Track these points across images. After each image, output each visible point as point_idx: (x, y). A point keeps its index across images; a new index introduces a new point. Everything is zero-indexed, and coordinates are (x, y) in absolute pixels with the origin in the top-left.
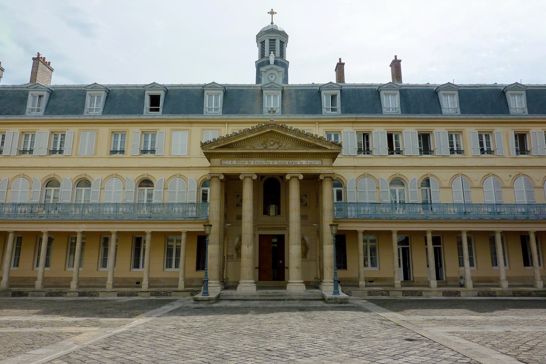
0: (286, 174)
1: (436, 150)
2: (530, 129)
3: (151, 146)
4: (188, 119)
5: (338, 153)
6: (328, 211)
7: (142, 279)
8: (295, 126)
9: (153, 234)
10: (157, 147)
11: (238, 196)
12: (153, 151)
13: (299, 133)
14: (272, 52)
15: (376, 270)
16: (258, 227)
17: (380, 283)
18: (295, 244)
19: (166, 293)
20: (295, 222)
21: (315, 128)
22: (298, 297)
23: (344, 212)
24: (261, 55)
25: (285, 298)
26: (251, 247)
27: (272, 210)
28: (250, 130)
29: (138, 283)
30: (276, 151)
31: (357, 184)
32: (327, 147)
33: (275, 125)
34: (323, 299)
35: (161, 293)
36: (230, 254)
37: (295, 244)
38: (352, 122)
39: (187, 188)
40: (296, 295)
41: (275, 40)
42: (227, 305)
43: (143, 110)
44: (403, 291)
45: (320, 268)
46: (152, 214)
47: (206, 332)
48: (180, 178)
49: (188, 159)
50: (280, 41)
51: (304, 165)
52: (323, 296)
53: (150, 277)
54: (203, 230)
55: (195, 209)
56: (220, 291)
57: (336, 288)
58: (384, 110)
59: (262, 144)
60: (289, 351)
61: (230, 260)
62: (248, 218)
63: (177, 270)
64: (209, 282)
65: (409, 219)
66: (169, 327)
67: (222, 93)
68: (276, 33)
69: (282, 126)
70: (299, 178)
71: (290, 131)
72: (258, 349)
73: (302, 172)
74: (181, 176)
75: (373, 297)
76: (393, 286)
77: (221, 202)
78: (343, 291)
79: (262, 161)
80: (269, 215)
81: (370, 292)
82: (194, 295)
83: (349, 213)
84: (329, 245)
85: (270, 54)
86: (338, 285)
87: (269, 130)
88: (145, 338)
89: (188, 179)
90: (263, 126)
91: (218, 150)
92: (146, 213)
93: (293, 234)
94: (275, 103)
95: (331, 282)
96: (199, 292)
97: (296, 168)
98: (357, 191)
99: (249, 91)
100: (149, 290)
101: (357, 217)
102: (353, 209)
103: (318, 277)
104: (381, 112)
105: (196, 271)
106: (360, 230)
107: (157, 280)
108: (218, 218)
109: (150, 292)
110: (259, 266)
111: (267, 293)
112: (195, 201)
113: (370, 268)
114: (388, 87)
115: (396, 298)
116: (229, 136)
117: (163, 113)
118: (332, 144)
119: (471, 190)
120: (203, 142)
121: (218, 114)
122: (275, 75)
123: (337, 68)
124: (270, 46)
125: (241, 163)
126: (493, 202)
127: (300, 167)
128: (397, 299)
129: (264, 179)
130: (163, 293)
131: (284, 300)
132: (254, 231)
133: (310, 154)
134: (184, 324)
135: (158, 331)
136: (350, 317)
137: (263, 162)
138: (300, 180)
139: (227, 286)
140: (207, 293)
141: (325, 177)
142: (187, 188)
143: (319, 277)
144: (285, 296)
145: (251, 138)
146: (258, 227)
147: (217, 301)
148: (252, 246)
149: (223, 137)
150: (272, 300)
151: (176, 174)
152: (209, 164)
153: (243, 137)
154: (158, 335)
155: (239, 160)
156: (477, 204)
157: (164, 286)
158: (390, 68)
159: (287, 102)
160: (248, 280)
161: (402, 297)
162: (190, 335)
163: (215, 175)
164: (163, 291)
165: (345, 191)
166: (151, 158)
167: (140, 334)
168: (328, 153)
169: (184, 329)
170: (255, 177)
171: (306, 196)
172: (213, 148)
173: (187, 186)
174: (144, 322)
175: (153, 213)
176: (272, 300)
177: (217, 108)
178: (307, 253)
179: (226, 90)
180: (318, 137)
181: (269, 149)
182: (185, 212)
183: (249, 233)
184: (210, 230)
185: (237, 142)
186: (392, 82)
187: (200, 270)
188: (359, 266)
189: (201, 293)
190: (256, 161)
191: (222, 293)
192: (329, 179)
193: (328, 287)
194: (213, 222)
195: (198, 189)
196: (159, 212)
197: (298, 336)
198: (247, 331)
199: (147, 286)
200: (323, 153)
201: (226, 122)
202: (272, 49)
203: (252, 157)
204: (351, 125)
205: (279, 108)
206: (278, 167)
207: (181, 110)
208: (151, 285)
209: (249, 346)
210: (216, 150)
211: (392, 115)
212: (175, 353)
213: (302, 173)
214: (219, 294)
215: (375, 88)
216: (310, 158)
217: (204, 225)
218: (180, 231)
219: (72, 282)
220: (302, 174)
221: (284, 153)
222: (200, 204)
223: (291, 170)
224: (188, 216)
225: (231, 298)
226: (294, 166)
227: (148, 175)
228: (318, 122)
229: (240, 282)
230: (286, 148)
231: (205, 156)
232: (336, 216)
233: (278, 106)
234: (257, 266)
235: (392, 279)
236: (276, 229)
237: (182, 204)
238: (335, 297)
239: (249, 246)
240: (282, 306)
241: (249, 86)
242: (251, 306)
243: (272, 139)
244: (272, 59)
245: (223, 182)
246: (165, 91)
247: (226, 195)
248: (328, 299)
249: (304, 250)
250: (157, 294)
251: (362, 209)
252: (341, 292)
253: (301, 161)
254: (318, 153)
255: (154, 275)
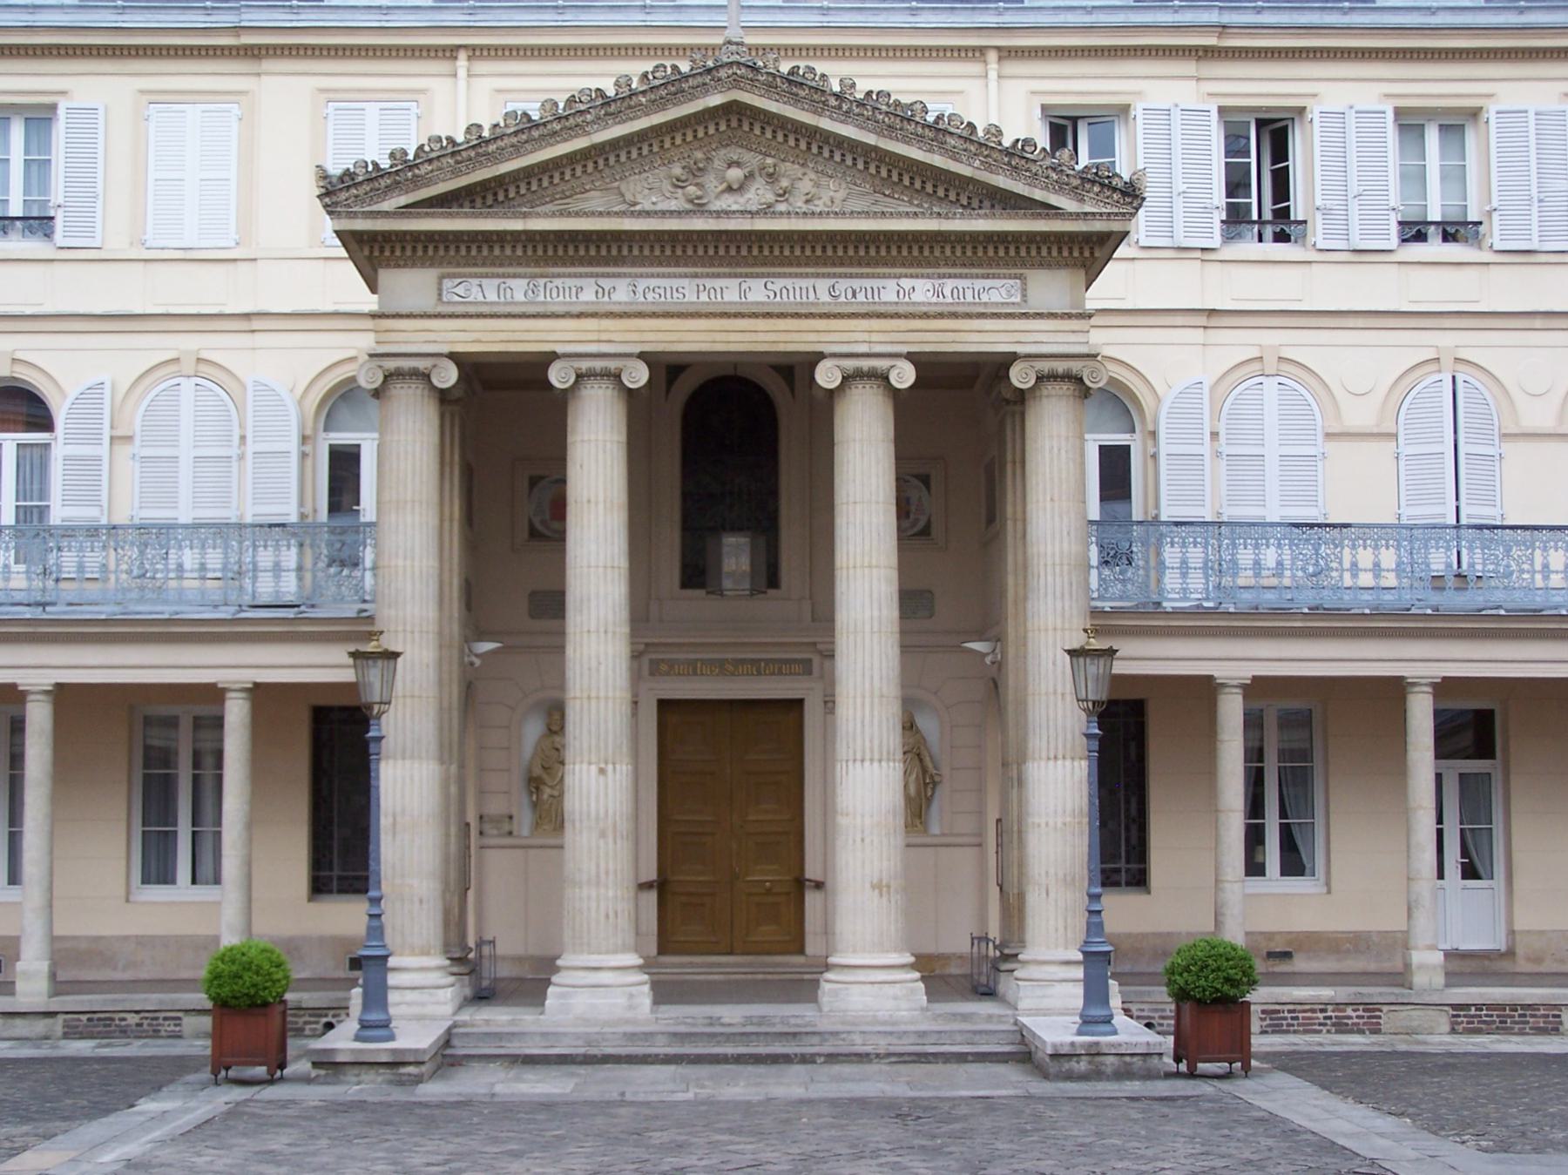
1: (1495, 216)
2: (1491, 92)
3: (27, 191)
4: (237, 30)
8: (869, 78)
10: (61, 200)
11: (534, 482)
13: (902, 118)
16: (651, 661)
17: (1330, 965)
18: (868, 757)
19: (153, 1019)
21: (979, 83)
22: (882, 1045)
23: (1141, 572)
26: (620, 775)
28: (608, 102)
31: (1216, 414)
32: (1054, 199)
34: (1024, 1054)
35: (124, 1019)
36: (496, 806)
39: (243, 438)
40: (871, 1033)
44: (1455, 1007)
46: (50, 583)
48: (199, 381)
49: (239, 263)
52: (1022, 1035)
53: (58, 932)
54: (348, 676)
55: (290, 557)
56: (448, 1009)
57: (1095, 993)
59: (679, 184)
61: (493, 841)
63: (204, 893)
64: (392, 962)
65: (1502, 612)
73: (905, 349)
74: (203, 368)
75: (1292, 1038)
76: (1401, 978)
77: (442, 520)
78: (1126, 1006)
79: (676, 283)
80: (719, 592)
81: (1278, 1011)
82: (303, 1030)
83: (1171, 581)
84: (1060, 762)
87: (715, 100)
90: (686, 77)
91: (418, 216)
93: (859, 701)
95: (1068, 963)
96: (331, 1013)
97: (875, 324)
98: (1218, 454)
100: (56, 1004)
101: (1211, 604)
102: (1196, 555)
103: (991, 936)
105: (310, 900)
106: (1414, 674)
107: (93, 951)
109: (61, 1018)
111: (712, 1021)
112: (289, 512)
113: (1274, 881)
115: (1419, 1043)
116: (486, 134)
118: (1088, 186)
119: (1508, 448)
120: (335, 170)
125: (554, 295)
126: (1444, 516)
127: (897, 316)
128: (1421, 1048)
129: (686, 385)
130: (133, 1019)
131: (806, 1059)
132: (636, 678)
133: (959, 242)
137: (685, 289)
139: (485, 983)
140: (385, 1025)
141: (1041, 379)
142: (243, 438)
143: (994, 932)
144: (816, 1040)
145: (614, 145)
146: (651, 661)
147: (439, 1068)
149: (451, 140)
150: (739, 1059)
151: (1255, 353)
152: (370, 302)
153: (566, 140)
155: (542, 276)
156: (1369, 526)
161: (1448, 1039)
163: (406, 364)
165: (1152, 451)
168: (1060, 239)
170: (638, 376)
171: (925, 480)
172: (388, 205)
173: (242, 426)
175: (57, 580)
176: (739, 1059)
178: (929, 800)
181: (719, 214)
184: (390, 682)
187: (330, 892)
188: (1217, 875)
190: (642, 284)
191: (465, 1024)
195: (304, 439)
196: (88, 576)
199: (42, 985)
200: (1032, 238)
201: (459, 47)
203: (619, 261)
204: (1189, 67)
206: (768, 315)
213: (642, 353)
216: (954, 265)
217: (355, 655)
219: (18, 964)
220: (910, 357)
221: (804, 237)
222: (317, 526)
223: (845, 336)
224: (254, 597)
226: (863, 310)
228: (999, 49)
229: (559, 962)
231: (343, 253)
232: (1101, 598)
235: (1401, 942)
236: (758, 668)
237: (222, 531)
238: (1092, 1045)
239: (610, 767)
240: (798, 1092)
242: (629, 1097)
243: (735, 153)
245: (450, 402)
248: (1056, 1056)
250: (100, 1025)
251: (1245, 557)
252: (1120, 1019)
253: (906, 283)
255: (77, 925)
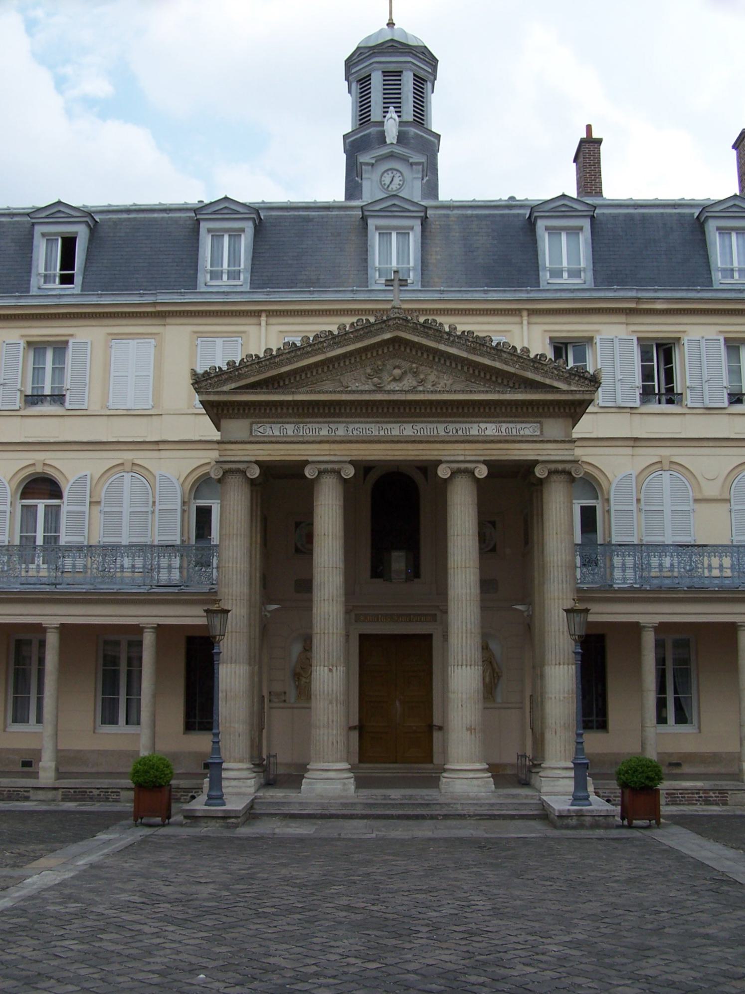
0: (440, 462)
4: (155, 304)
5: (590, 402)
6: (560, 569)
7: (38, 753)
8: (464, 325)
9: (64, 630)
10: (68, 387)
12: (58, 398)
13: (480, 344)
14: (392, 109)
15: (691, 731)
16: (356, 615)
18: (464, 663)
20: (464, 602)
22: (472, 810)
24: (361, 115)
25: (438, 812)
26: (339, 672)
27: (398, 561)
28: (335, 337)
29: (27, 764)
30: (411, 397)
31: (639, 491)
32: (556, 384)
33: (404, 320)
34: (544, 815)
35: (91, 792)
37: (464, 663)
38: (626, 309)
39: (154, 502)
41: (401, 72)
42: (277, 831)
43: (30, 280)
45: (532, 729)
47: (232, 914)
50: (415, 75)
51: (489, 436)
52: (543, 805)
54: (203, 621)
55: (176, 562)
57: (580, 784)
58: (717, 277)
59: (369, 377)
60: (473, 979)
62: (331, 590)
63: (131, 729)
64: (224, 765)
66: (128, 899)
67: (249, 227)
68: (403, 54)
69: (425, 325)
70: (476, 475)
71: (449, 339)
72: (383, 972)
73: (482, 458)
74: (136, 468)
77: (251, 544)
78: (597, 791)
81: (674, 794)
82: (180, 799)
83: (617, 574)
84: (561, 666)
85: (384, 112)
86: (586, 776)
87: (387, 336)
88: (68, 931)
89: (155, 477)
90: (372, 325)
92: (44, 573)
94: (403, 253)
96: (194, 791)
97: (467, 446)
99: (325, 220)
103: (528, 755)
104: (709, 282)
105: (184, 734)
107: (77, 757)
108: (246, 590)
110: (360, 720)
113: (672, 726)
114: (728, 208)
116: (274, 353)
117: (86, 287)
118: (573, 377)
120: (200, 370)
121: (239, 289)
122: (400, 172)
123: (581, 154)
124: (399, 82)
129: (373, 477)
130: (96, 792)
131: (432, 817)
132: (347, 623)
134: (167, 890)
135: (100, 909)
136: (625, 872)
137: (373, 429)
138: (478, 481)
140: (221, 797)
142: (154, 502)
143: (529, 753)
144: (438, 807)
145: (338, 358)
147: (247, 820)
148: (342, 669)
149: (257, 356)
152: (216, 435)
154: (102, 923)
155: (301, 423)
157: (98, 775)
158: (734, 152)
159: (436, 255)
160: (333, 762)
162: (189, 925)
164: (98, 789)
165: (607, 508)
166: (66, 418)
167: (52, 919)
169: (169, 906)
171: (493, 524)
172: (226, 388)
173: (154, 497)
174: (57, 882)
175: (62, 572)
176: (399, 817)
177: (234, 271)
178: (496, 685)
179: (262, 217)
180: (532, 356)
181: (389, 392)
182: (149, 570)
183: (333, 633)
185: (295, 372)
186: (738, 194)
189: (203, 798)
190: (351, 427)
191: (260, 798)
192: (562, 477)
193: (557, 783)
194: (230, 602)
195: (184, 503)
197: (487, 929)
198: (345, 914)
201: (261, 311)
202: (392, 98)
203: (339, 415)
204: (622, 318)
205: (414, 269)
206: (414, 442)
207: (134, 280)
208: (62, 770)
209: (359, 961)
210: (236, 393)
211: (740, 290)
212: (156, 979)
214: (253, 800)
215: (692, 211)
218: (138, 625)
220: (485, 462)
223: (452, 452)
225: (287, 812)
227: (45, 464)
230: (429, 387)
231: (204, 411)
232: (581, 583)
233: (412, 264)
234: (355, 721)
239: (335, 668)
240: (429, 834)
241: (327, 207)
242: (343, 836)
243: (397, 362)
244: (391, 129)
246: (89, 226)
247: (265, 520)
248: (561, 817)
249: (487, 679)
250: (81, 795)
251: (655, 561)
252: (593, 798)
253: (483, 426)
254: (531, 403)
